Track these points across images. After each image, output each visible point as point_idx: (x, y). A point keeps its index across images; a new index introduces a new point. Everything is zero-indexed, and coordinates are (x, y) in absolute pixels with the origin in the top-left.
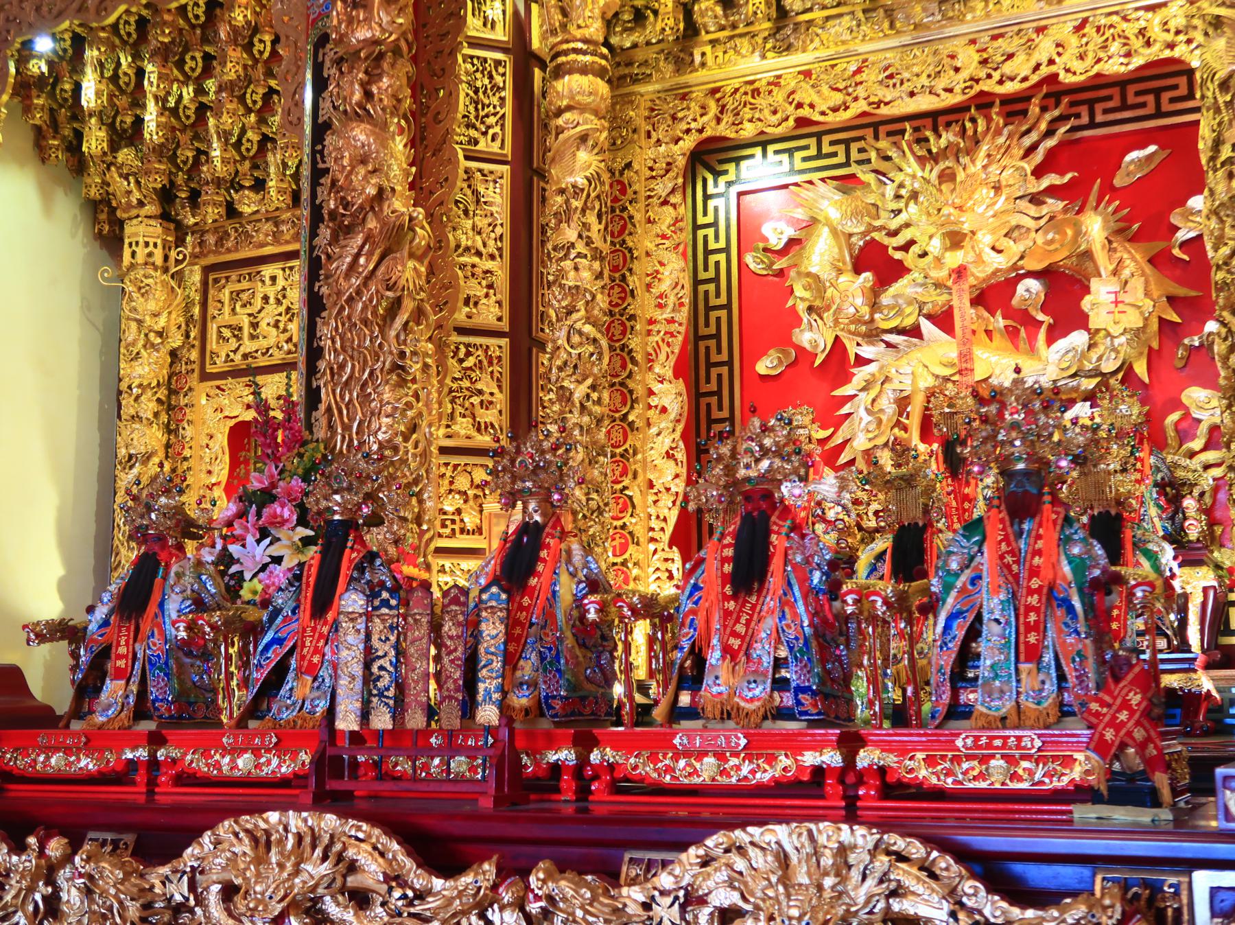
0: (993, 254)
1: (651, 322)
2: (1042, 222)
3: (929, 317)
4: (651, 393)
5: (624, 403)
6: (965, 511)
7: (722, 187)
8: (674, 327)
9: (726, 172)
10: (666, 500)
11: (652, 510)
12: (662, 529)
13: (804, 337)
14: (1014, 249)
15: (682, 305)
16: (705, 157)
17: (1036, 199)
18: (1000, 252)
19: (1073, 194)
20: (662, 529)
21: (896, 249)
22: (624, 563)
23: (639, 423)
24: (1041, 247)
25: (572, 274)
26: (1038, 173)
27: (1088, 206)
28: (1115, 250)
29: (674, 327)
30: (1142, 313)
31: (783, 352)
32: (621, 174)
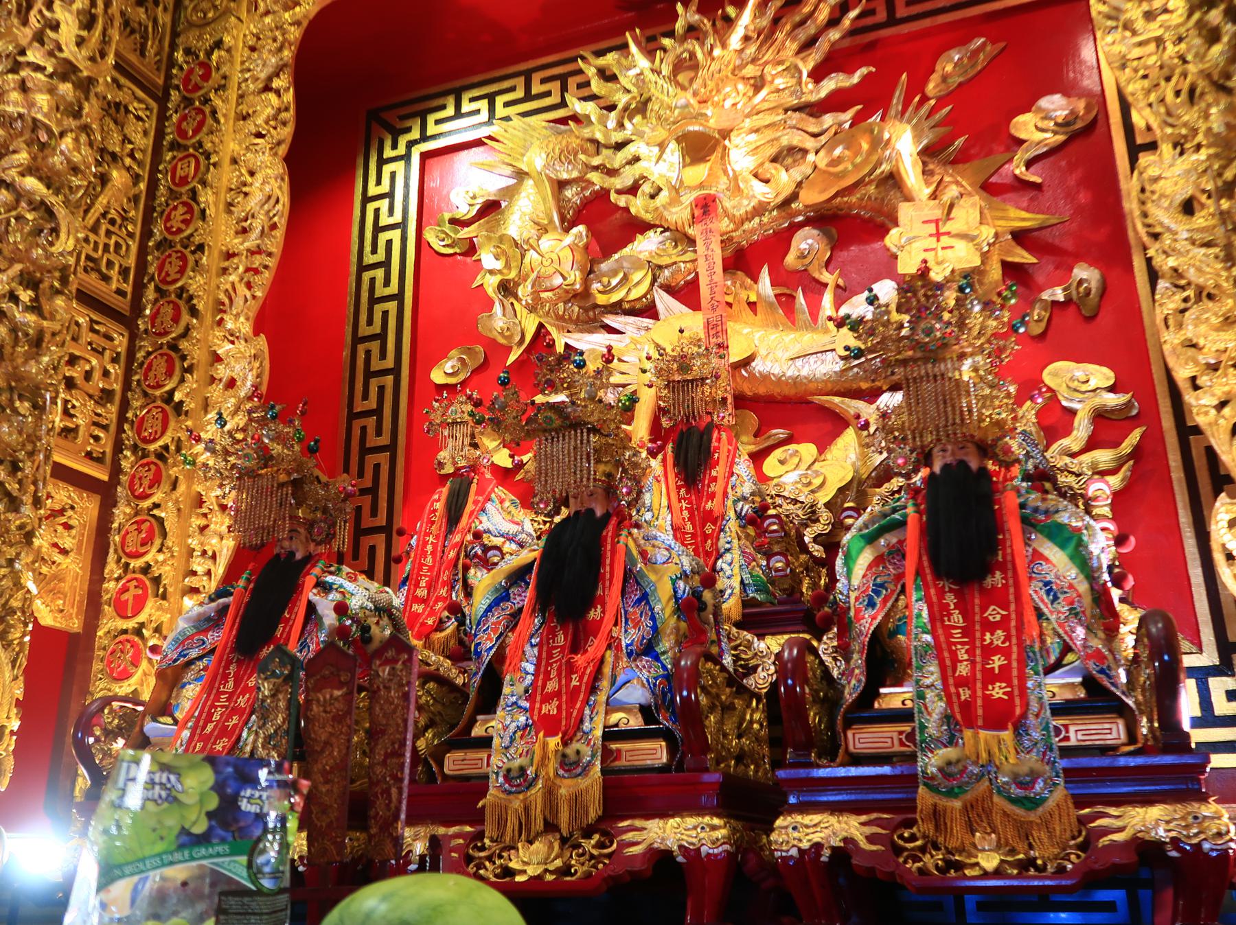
0: (756, 183)
1: (229, 256)
2: (823, 139)
3: (668, 289)
4: (217, 359)
5: (170, 373)
6: (706, 537)
7: (401, 150)
8: (257, 261)
9: (409, 130)
10: (221, 523)
11: (194, 542)
12: (209, 573)
13: (497, 321)
14: (785, 179)
15: (274, 227)
16: (385, 116)
17: (816, 109)
18: (767, 181)
19: (869, 101)
20: (209, 573)
21: (619, 192)
22: (138, 632)
23: (190, 405)
24: (826, 162)
25: (15, 96)
26: (818, 75)
27: (892, 112)
28: (932, 173)
29: (257, 261)
30: (978, 247)
31: (469, 352)
32: (209, 54)
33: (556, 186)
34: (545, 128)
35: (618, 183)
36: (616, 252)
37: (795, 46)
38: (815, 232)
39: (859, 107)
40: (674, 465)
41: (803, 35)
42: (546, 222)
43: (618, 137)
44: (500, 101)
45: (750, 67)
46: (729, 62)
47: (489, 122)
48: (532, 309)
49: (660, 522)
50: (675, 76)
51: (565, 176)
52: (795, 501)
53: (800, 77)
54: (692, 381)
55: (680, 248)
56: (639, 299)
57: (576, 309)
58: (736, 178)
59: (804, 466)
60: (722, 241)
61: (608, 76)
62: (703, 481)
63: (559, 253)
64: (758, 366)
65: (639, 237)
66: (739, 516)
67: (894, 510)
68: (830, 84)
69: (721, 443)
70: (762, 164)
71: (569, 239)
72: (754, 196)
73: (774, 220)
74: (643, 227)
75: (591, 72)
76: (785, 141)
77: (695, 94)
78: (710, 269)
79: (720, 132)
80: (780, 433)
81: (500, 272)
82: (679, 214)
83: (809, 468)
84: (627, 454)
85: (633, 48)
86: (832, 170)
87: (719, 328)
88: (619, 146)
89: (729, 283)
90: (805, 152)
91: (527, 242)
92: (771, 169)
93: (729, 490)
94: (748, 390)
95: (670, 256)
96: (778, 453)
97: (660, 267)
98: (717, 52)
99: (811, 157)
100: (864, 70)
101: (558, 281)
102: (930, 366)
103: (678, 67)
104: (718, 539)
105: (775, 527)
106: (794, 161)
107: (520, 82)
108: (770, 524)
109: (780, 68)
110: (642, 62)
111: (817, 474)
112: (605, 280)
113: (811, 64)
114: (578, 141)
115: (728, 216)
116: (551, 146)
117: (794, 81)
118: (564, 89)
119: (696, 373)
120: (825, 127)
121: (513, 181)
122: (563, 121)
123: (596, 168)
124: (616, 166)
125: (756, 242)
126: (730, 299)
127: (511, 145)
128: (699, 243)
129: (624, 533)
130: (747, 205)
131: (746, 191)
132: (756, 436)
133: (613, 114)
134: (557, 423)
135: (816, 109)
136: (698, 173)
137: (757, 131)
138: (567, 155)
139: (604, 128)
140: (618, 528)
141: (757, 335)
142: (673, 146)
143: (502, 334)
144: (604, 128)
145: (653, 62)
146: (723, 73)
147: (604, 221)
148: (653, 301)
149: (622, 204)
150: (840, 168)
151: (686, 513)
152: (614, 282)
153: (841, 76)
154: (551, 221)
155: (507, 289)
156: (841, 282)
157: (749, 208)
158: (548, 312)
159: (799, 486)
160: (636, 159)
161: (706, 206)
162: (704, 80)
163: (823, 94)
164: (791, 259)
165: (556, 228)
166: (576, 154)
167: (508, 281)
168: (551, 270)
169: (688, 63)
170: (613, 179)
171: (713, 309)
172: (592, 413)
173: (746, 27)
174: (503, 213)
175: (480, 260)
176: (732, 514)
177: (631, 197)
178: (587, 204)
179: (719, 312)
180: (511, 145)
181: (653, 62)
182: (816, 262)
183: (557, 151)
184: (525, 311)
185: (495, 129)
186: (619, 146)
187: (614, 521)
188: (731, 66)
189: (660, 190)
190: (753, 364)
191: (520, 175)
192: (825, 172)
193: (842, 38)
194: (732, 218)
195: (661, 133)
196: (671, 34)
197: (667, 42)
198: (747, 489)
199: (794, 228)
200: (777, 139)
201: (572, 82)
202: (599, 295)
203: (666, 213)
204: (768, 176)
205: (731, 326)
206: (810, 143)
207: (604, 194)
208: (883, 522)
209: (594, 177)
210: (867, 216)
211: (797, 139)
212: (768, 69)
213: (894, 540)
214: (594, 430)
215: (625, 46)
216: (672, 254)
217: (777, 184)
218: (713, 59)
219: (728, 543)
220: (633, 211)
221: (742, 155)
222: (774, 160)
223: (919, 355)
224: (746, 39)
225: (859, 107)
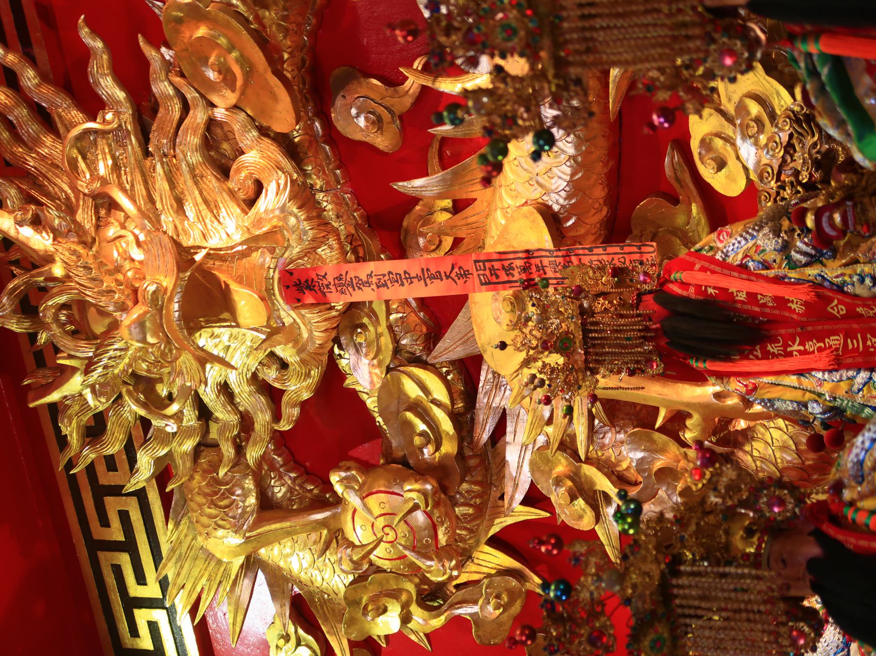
0: (262, 204)
2: (191, 95)
3: (433, 337)
6: (852, 315)
14: (256, 157)
17: (145, 108)
18: (259, 187)
21: (277, 416)
26: (92, 105)
33: (268, 514)
34: (177, 524)
35: (262, 418)
36: (374, 419)
37: (48, 140)
38: (339, 102)
39: (140, 38)
40: (732, 361)
41: (31, 128)
42: (325, 532)
43: (190, 417)
44: (135, 591)
45: (79, 217)
46: (74, 252)
47: (171, 613)
48: (465, 556)
49: (825, 389)
50: (96, 337)
51: (252, 500)
52: (789, 148)
53: (96, 132)
54: (585, 332)
55: (365, 320)
56: (448, 385)
57: (465, 486)
58: (256, 239)
59: (729, 130)
60: (358, 260)
61: (96, 429)
62: (754, 316)
63: (373, 516)
64: (557, 202)
65: (348, 382)
66: (813, 260)
67: (814, 73)
68: (109, 87)
69: (691, 281)
70: (232, 193)
71: (353, 500)
72: (283, 209)
73: (320, 170)
74: (333, 377)
75: (90, 455)
76: (195, 158)
77: (123, 308)
78: (398, 279)
79: (181, 269)
80: (671, 160)
81: (405, 606)
82: (311, 325)
83: (730, 120)
84: (713, 499)
85: (54, 397)
86: (239, 83)
87: (497, 265)
88: (204, 413)
89: (421, 241)
90: (211, 123)
91: (356, 564)
92: (240, 178)
93: (771, 273)
94: (597, 216)
95: (378, 336)
96: (707, 172)
97: (397, 350)
98: (58, 270)
99: (220, 113)
100: (85, 33)
101: (419, 517)
102: (566, 25)
103: (80, 331)
104: (856, 296)
105: (837, 217)
106: (227, 139)
107: (106, 558)
108: (832, 224)
109: (82, 165)
110: (75, 384)
111: (741, 108)
112: (417, 441)
113: (76, 115)
114: (197, 477)
115: (315, 249)
116: (204, 520)
117: (102, 143)
118: (117, 491)
119: (572, 326)
120: (171, 91)
121: (261, 576)
122: (166, 500)
123: (240, 450)
124: (234, 419)
125: (355, 194)
126: (448, 242)
127: (203, 581)
128: (358, 296)
129: (850, 513)
130: (297, 219)
131: (275, 222)
132: (675, 201)
133: (156, 423)
134: (663, 630)
135: (145, 108)
136: (246, 302)
137: (179, 203)
138: (219, 493)
139: (176, 422)
140: (838, 520)
141: (508, 201)
142: (203, 339)
143: (506, 607)
144: (176, 422)
145: (74, 370)
146: (90, 261)
147: (327, 439)
148: (452, 363)
149: (296, 411)
150: (237, 70)
151: (810, 346)
152: (421, 426)
153: (94, 67)
154: (323, 523)
155: (432, 596)
156: (418, 64)
157: (302, 215)
158: (470, 531)
159: (763, 139)
160: (225, 389)
161: (299, 286)
162: (101, 293)
163: (121, 95)
164: (382, 142)
165: (334, 516)
166: (220, 483)
167: (420, 593)
168: (402, 529)
169: (75, 312)
170: (257, 427)
171: (465, 275)
172: (647, 574)
173: (20, 223)
174: (311, 594)
175: (387, 637)
176: (812, 272)
177: (285, 399)
178: (295, 461)
179: (470, 266)
180: (203, 581)
181: (74, 370)
182: (388, 102)
183: (213, 511)
184: (471, 567)
185: (181, 603)
186: (204, 413)
187: (830, 530)
188: (80, 249)
189: (272, 355)
190: (556, 208)
191: (252, 564)
192: (242, 93)
193: (33, 62)
194: (317, 242)
195: (186, 360)
196: (33, 337)
197: (43, 338)
198: (768, 243)
199: (332, 135)
200: (192, 169)
201: (106, 478)
202: (443, 450)
203: (311, 348)
204: (250, 183)
205: (493, 244)
206: (199, 116)
207: (280, 439)
208: (835, 98)
209: (253, 454)
210: (314, 21)
211: (192, 139)
212: (82, 186)
213: (867, 80)
214: (675, 563)
215: (53, 408)
216: (378, 331)
217: (263, 169)
218: (68, 277)
219: (862, 280)
220: (306, 396)
221: (219, 229)
222: (224, 172)
223: (546, 41)
224: (37, 223)
225: (140, 38)
